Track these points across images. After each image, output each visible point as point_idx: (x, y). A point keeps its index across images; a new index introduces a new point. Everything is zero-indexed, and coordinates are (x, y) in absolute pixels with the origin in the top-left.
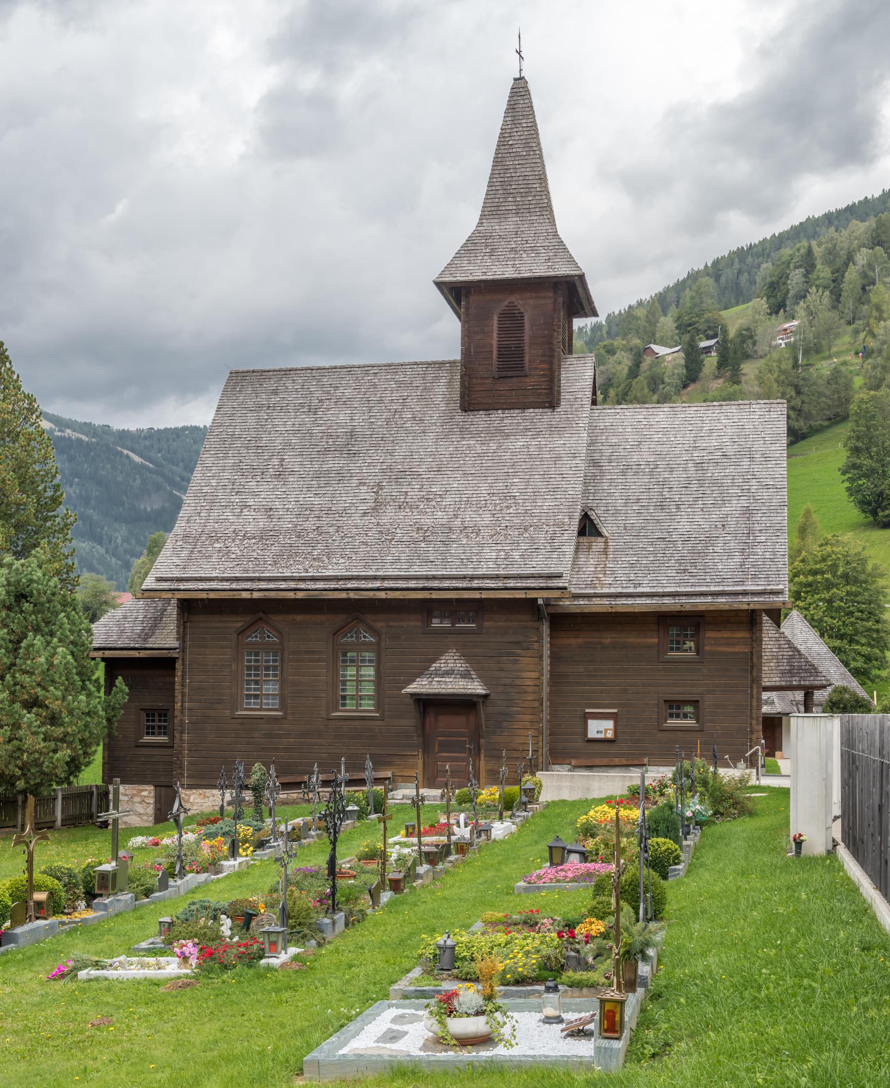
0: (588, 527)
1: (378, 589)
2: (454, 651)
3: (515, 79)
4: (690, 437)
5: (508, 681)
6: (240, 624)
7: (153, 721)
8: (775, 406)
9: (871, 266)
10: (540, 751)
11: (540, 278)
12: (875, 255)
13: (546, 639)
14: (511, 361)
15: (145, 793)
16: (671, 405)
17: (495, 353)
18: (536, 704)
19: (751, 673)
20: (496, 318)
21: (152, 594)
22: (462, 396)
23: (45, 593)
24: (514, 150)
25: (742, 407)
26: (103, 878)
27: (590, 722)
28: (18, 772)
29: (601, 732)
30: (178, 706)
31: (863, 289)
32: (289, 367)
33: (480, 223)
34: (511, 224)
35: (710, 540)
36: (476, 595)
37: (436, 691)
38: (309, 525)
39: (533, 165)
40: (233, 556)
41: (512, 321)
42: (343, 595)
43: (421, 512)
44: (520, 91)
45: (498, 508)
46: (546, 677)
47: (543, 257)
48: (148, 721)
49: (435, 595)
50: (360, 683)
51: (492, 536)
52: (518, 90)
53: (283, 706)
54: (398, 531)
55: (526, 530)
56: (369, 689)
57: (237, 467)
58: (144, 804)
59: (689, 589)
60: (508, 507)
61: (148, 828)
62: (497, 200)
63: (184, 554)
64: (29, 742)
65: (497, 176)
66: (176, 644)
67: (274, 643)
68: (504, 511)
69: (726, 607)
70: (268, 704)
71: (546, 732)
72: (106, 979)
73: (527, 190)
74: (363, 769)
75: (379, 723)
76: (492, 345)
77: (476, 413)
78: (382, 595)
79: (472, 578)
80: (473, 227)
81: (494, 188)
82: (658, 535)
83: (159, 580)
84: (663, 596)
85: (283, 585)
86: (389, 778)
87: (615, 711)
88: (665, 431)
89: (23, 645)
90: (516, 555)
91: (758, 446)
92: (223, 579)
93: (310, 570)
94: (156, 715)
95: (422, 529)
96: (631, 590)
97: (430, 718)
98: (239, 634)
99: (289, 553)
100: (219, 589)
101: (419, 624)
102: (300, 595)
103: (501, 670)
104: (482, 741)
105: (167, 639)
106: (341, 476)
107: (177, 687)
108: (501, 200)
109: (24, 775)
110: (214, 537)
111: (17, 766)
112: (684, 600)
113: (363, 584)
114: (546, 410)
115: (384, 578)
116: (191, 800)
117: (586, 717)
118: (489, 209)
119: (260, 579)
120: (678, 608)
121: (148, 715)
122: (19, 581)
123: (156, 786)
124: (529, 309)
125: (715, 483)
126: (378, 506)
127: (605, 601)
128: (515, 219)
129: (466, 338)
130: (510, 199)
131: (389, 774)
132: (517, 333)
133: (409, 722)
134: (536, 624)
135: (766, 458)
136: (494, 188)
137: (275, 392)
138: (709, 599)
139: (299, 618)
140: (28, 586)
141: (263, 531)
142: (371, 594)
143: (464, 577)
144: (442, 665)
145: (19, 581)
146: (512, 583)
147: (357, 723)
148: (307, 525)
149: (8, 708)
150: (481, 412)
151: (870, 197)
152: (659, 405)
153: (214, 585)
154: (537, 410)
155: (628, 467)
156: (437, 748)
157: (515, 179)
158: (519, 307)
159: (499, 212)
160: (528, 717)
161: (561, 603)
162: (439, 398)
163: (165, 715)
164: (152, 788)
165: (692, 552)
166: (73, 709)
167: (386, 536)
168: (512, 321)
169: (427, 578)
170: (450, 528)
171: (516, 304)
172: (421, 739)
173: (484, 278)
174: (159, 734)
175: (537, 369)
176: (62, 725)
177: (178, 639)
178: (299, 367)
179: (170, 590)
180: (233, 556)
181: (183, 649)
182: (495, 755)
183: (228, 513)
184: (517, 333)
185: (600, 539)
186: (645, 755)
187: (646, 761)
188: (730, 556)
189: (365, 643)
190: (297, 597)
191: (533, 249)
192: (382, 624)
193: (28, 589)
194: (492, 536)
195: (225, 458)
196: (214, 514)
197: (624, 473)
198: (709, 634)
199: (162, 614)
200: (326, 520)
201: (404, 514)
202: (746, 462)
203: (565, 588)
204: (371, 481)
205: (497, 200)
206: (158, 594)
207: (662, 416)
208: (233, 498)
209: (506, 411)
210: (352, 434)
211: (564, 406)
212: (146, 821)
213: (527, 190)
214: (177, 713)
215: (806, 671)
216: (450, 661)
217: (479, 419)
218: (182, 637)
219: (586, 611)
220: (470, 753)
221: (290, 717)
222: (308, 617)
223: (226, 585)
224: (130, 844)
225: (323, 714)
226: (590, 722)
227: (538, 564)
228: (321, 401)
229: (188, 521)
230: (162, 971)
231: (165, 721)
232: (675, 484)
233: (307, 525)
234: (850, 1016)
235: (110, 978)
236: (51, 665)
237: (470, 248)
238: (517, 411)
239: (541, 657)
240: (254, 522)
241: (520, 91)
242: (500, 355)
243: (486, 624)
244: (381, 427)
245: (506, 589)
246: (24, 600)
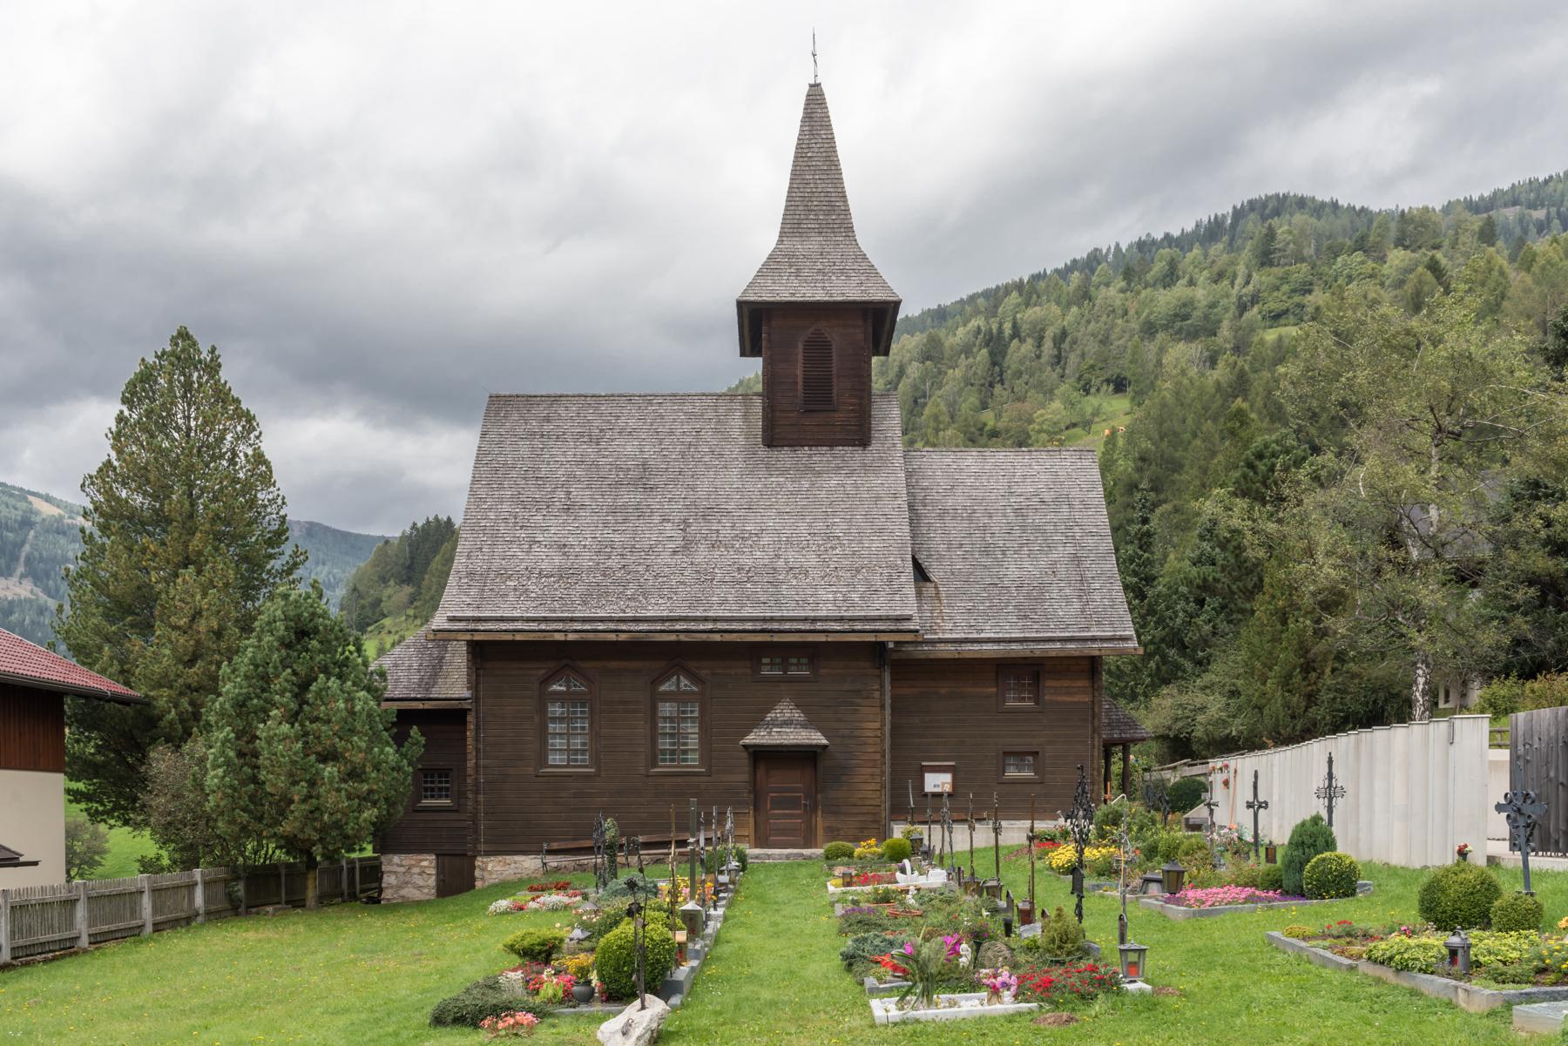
0: (921, 574)
1: (711, 631)
4: (1003, 482)
5: (846, 732)
6: (542, 672)
13: (888, 687)
14: (818, 395)
15: (425, 863)
17: (800, 386)
18: (878, 756)
20: (801, 347)
21: (446, 635)
28: (315, 836)
30: (471, 764)
33: (780, 241)
36: (822, 638)
38: (614, 562)
41: (818, 350)
42: (673, 637)
43: (737, 551)
44: (815, 101)
47: (854, 281)
50: (683, 736)
53: (596, 761)
56: (693, 742)
57: (517, 499)
60: (833, 548)
63: (473, 592)
64: (331, 799)
66: (466, 694)
67: (582, 693)
69: (1077, 654)
72: (917, 1021)
78: (717, 637)
79: (815, 620)
82: (988, 581)
83: (452, 619)
85: (601, 627)
88: (977, 476)
91: (1075, 493)
92: (529, 620)
96: (975, 636)
97: (761, 773)
100: (527, 631)
103: (839, 720)
105: (455, 685)
106: (641, 512)
107: (470, 741)
109: (321, 840)
110: (504, 575)
111: (315, 829)
112: (1032, 646)
113: (692, 626)
117: (923, 770)
119: (572, 620)
120: (1028, 654)
122: (299, 616)
124: (837, 336)
125: (1038, 529)
126: (687, 546)
127: (950, 647)
133: (740, 776)
134: (877, 672)
137: (548, 419)
138: (1058, 645)
139: (613, 664)
141: (560, 568)
142: (704, 637)
143: (805, 619)
145: (299, 616)
146: (859, 626)
147: (679, 779)
148: (609, 563)
153: (519, 625)
160: (869, 771)
162: (736, 433)
165: (1029, 596)
167: (705, 577)
168: (818, 350)
169: (764, 620)
174: (440, 797)
181: (476, 699)
183: (515, 549)
184: (817, 360)
188: (1068, 602)
191: (842, 272)
195: (499, 489)
196: (499, 550)
197: (941, 517)
198: (1049, 683)
200: (630, 559)
202: (1065, 509)
206: (453, 635)
207: (969, 461)
210: (644, 466)
211: (875, 446)
214: (470, 771)
216: (785, 710)
217: (785, 456)
218: (474, 685)
221: (603, 774)
222: (622, 664)
224: (492, 908)
227: (880, 606)
228: (602, 431)
230: (955, 1009)
232: (996, 530)
233: (609, 563)
236: (352, 713)
237: (772, 265)
240: (550, 561)
241: (815, 101)
243: (822, 671)
244: (676, 460)
245: (853, 631)
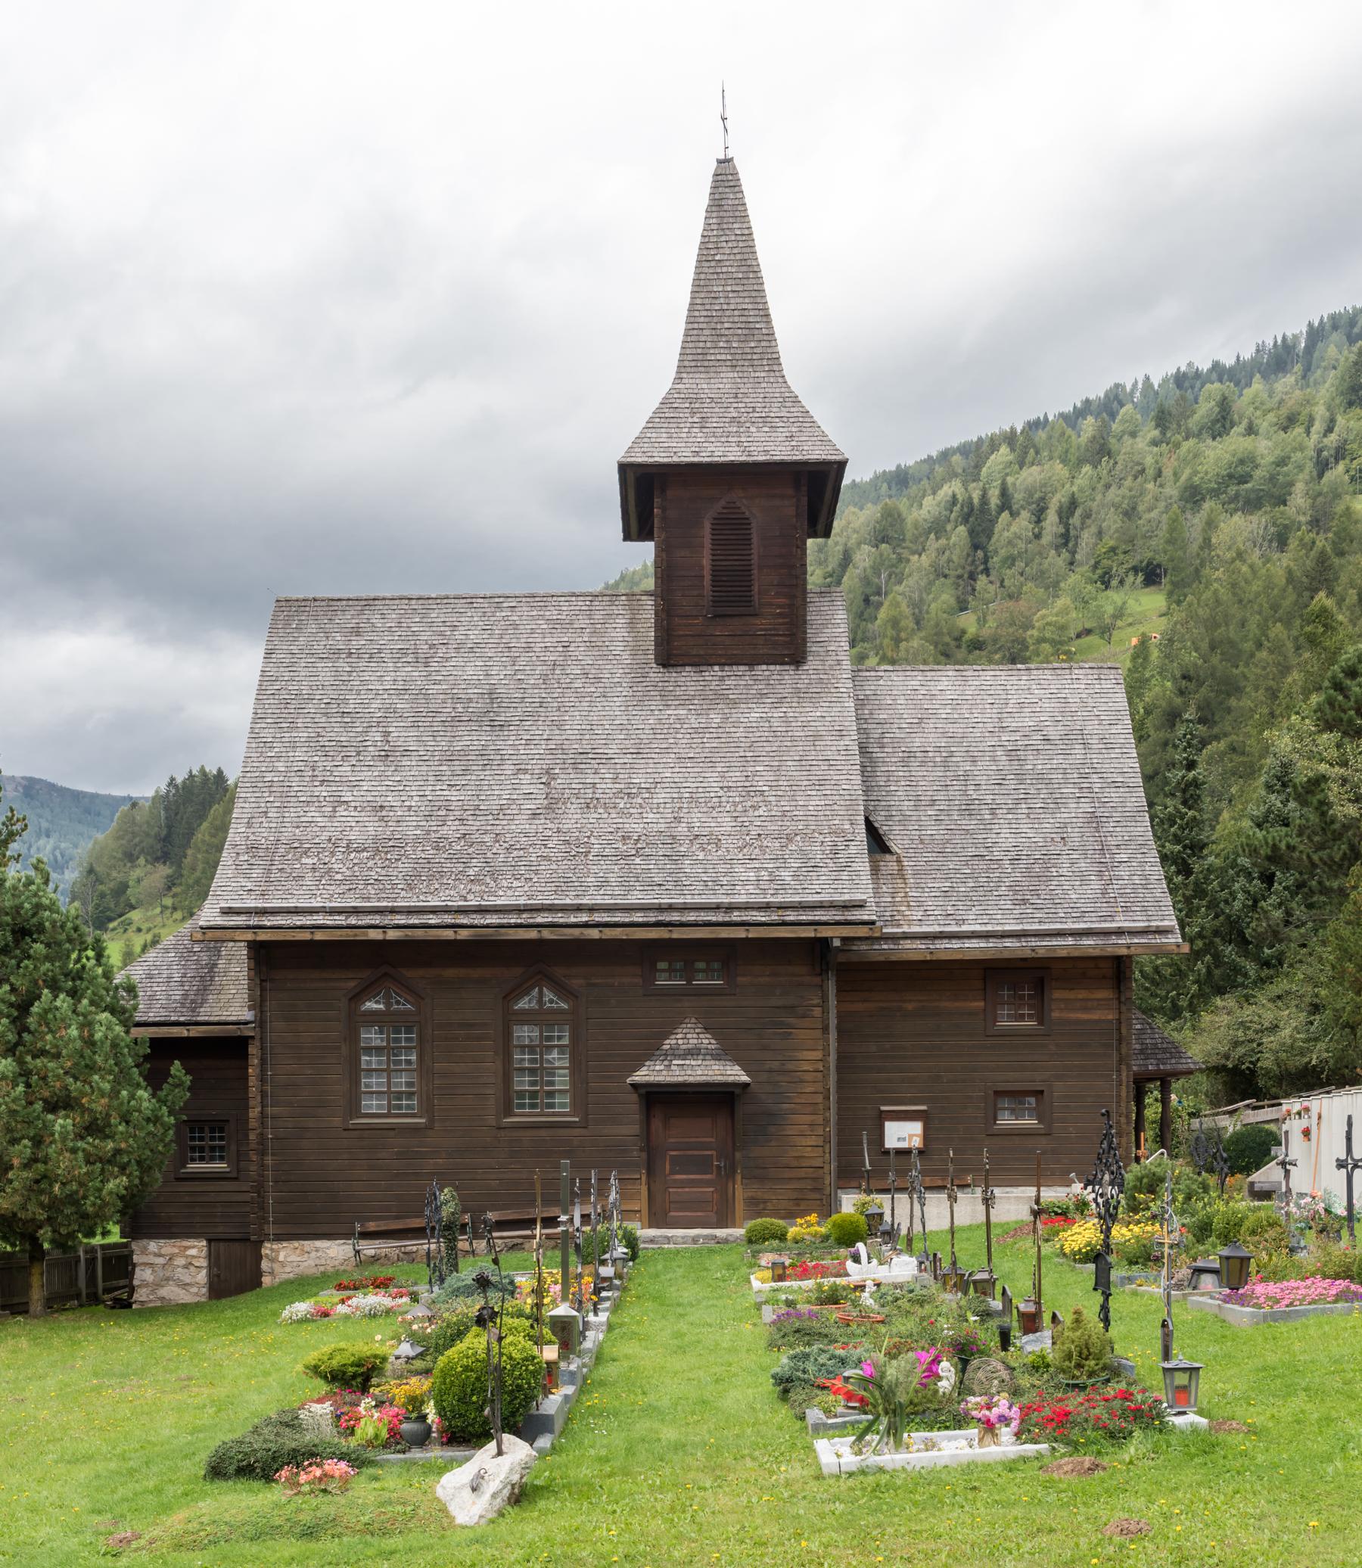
1: (586, 925)
2: (693, 1020)
3: (720, 162)
5: (775, 1065)
6: (352, 984)
7: (201, 1139)
8: (1106, 671)
9: (876, 570)
10: (827, 1167)
11: (782, 464)
12: (881, 555)
13: (832, 1002)
14: (732, 593)
15: (193, 1252)
16: (957, 667)
17: (707, 581)
18: (820, 1099)
19: (1119, 1050)
21: (218, 934)
22: (659, 642)
23: (62, 927)
24: (724, 270)
25: (1059, 672)
26: (563, 1329)
27: (888, 1124)
28: (42, 1215)
29: (904, 1139)
30: (254, 1113)
31: (867, 601)
32: (372, 595)
33: (679, 379)
34: (725, 382)
35: (1048, 860)
36: (740, 933)
37: (680, 1079)
38: (451, 830)
39: (754, 294)
40: (339, 877)
41: (732, 531)
42: (533, 934)
43: (621, 813)
44: (726, 183)
45: (740, 808)
46: (832, 1058)
48: (193, 1139)
49: (677, 934)
50: (548, 1071)
51: (741, 849)
52: (724, 178)
53: (427, 1108)
54: (593, 840)
55: (790, 840)
56: (562, 1080)
57: (315, 744)
58: (192, 1268)
59: (1036, 927)
60: (754, 808)
61: (197, 1304)
62: (701, 345)
63: (256, 873)
65: (699, 307)
66: (247, 1015)
68: (751, 813)
69: (1097, 953)
70: (399, 1107)
71: (833, 1140)
72: (881, 1470)
73: (745, 332)
74: (532, 1203)
75: (577, 1132)
76: (702, 568)
77: (679, 669)
78: (594, 934)
79: (730, 908)
80: (668, 385)
81: (696, 326)
82: (972, 851)
83: (227, 912)
84: (1003, 937)
87: (924, 1108)
88: (955, 704)
89: (35, 1009)
90: (786, 875)
91: (1091, 727)
93: (469, 897)
94: (207, 1129)
95: (629, 838)
96: (954, 928)
97: (657, 1124)
98: (350, 999)
99: (428, 873)
100: (330, 927)
101: (639, 980)
102: (464, 934)
103: (765, 1048)
104: (738, 1155)
105: (232, 1003)
107: (253, 1081)
108: (709, 345)
111: (41, 1205)
112: (1034, 942)
113: (560, 918)
114: (787, 667)
115: (592, 909)
116: (281, 1258)
117: (882, 1118)
118: (690, 357)
119: (393, 911)
120: (1028, 954)
121: (192, 1131)
123: (209, 1241)
124: (761, 513)
125: (1040, 778)
126: (552, 806)
128: (731, 375)
129: (664, 555)
130: (721, 344)
132: (731, 547)
133: (629, 1128)
135: (1109, 747)
136: (696, 326)
137: (357, 632)
138: (1070, 941)
139: (450, 973)
140: (34, 915)
142: (576, 933)
143: (717, 907)
144: (680, 1042)
145: (18, 908)
146: (791, 916)
147: (543, 1133)
149: (23, 1113)
150: (688, 669)
151: (858, 480)
152: (940, 667)
153: (319, 919)
154: (772, 667)
155: (910, 754)
157: (728, 313)
158: (743, 509)
159: (706, 364)
161: (855, 948)
162: (618, 648)
163: (221, 1130)
164: (204, 1243)
166: (129, 1112)
167: (577, 850)
168: (732, 531)
169: (660, 908)
170: (674, 837)
171: (738, 504)
172: (644, 1155)
173: (696, 459)
174: (212, 1159)
175: (771, 604)
176: (111, 1137)
177: (250, 1008)
178: (388, 595)
179: (248, 927)
180: (339, 877)
181: (261, 1022)
182: (758, 1174)
184: (731, 547)
185: (888, 857)
186: (968, 1171)
187: (969, 1179)
189: (552, 1011)
190: (459, 938)
192: (582, 981)
193: (34, 920)
194: (741, 849)
196: (291, 814)
197: (905, 762)
198: (1057, 994)
199: (211, 970)
200: (474, 825)
201: (596, 816)
202: (1078, 749)
203: (873, 923)
204: (537, 767)
205: (701, 345)
208: (317, 791)
209: (727, 668)
210: (492, 695)
211: (812, 663)
212: (197, 1294)
213: (745, 332)
215: (1165, 1051)
216: (689, 1036)
217: (687, 679)
218: (258, 1003)
219: (893, 958)
223: (340, 920)
224: (286, 1314)
225: (491, 1120)
226: (888, 1124)
227: (821, 888)
228: (432, 646)
229: (249, 825)
231: (221, 1139)
232: (982, 780)
235: (889, 1467)
236: (90, 1043)
237: (667, 412)
238: (742, 668)
239: (825, 1029)
240: (363, 829)
242: (715, 581)
244: (535, 686)
245: (784, 924)
246: (28, 939)
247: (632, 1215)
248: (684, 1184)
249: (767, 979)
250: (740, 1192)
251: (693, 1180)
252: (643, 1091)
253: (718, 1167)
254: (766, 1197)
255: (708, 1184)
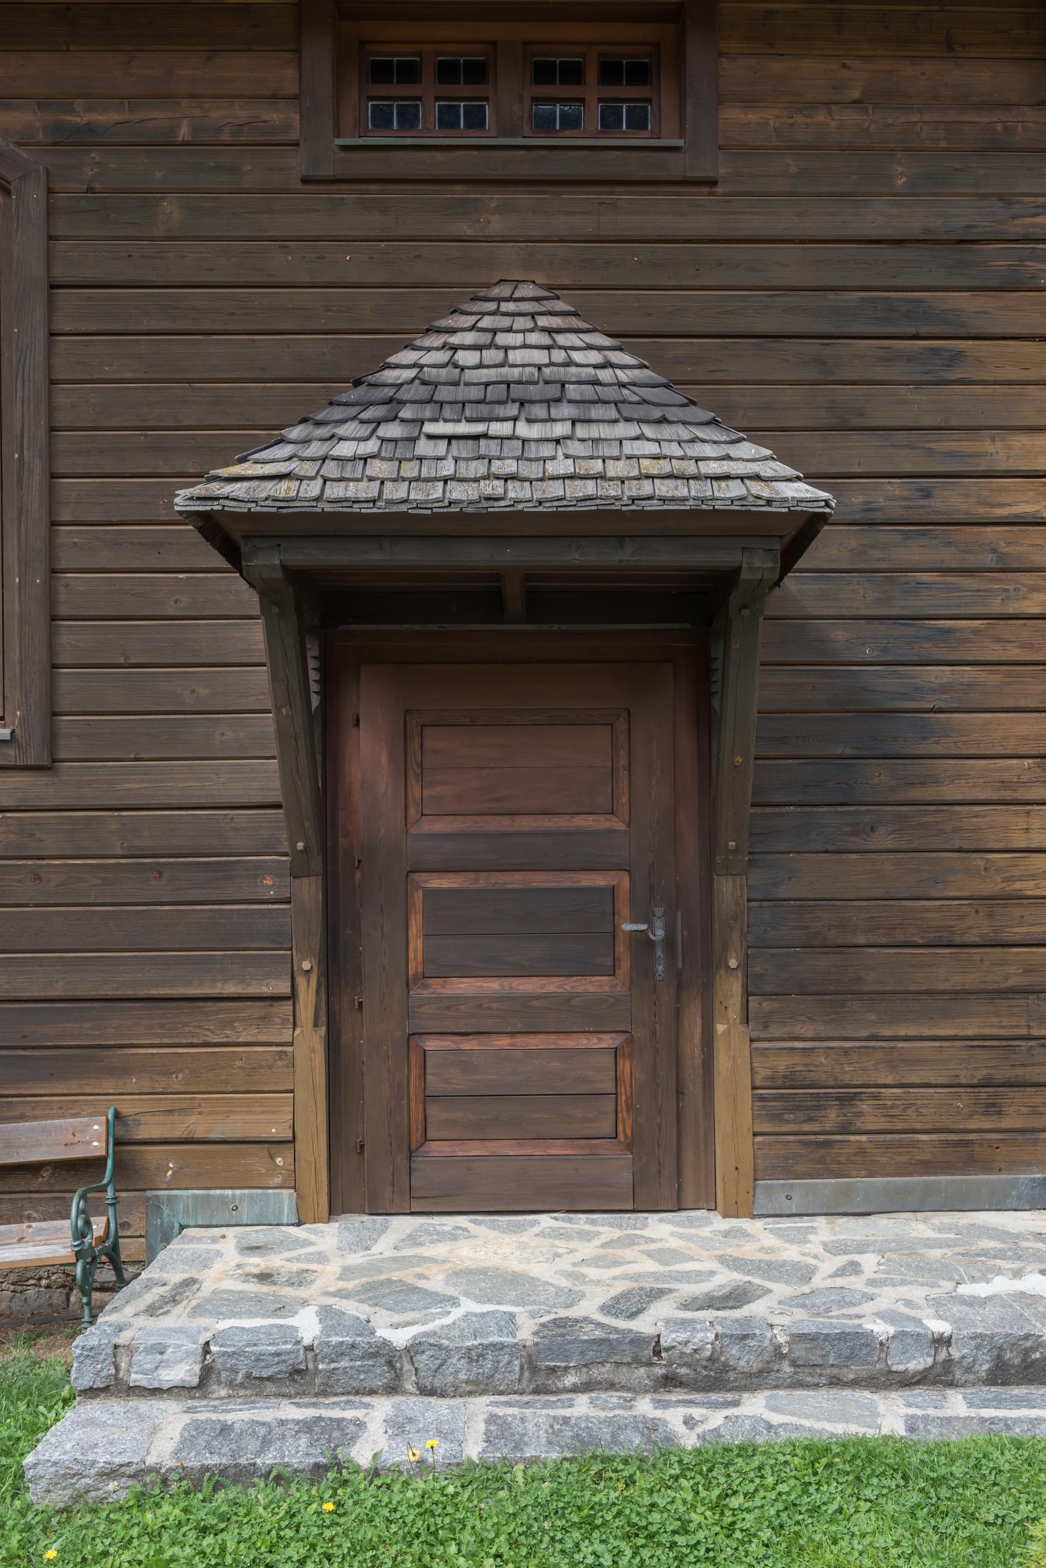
86: (91, 1166)
104: (728, 890)
131: (91, 1137)
156: (417, 945)
182: (819, 974)
220: (642, 972)
234: (1010, 1471)
247: (256, 1159)
248: (483, 1016)
249: (851, 117)
250: (736, 1056)
251: (567, 1000)
252: (268, 561)
253: (642, 944)
254: (849, 1072)
255: (590, 1016)
